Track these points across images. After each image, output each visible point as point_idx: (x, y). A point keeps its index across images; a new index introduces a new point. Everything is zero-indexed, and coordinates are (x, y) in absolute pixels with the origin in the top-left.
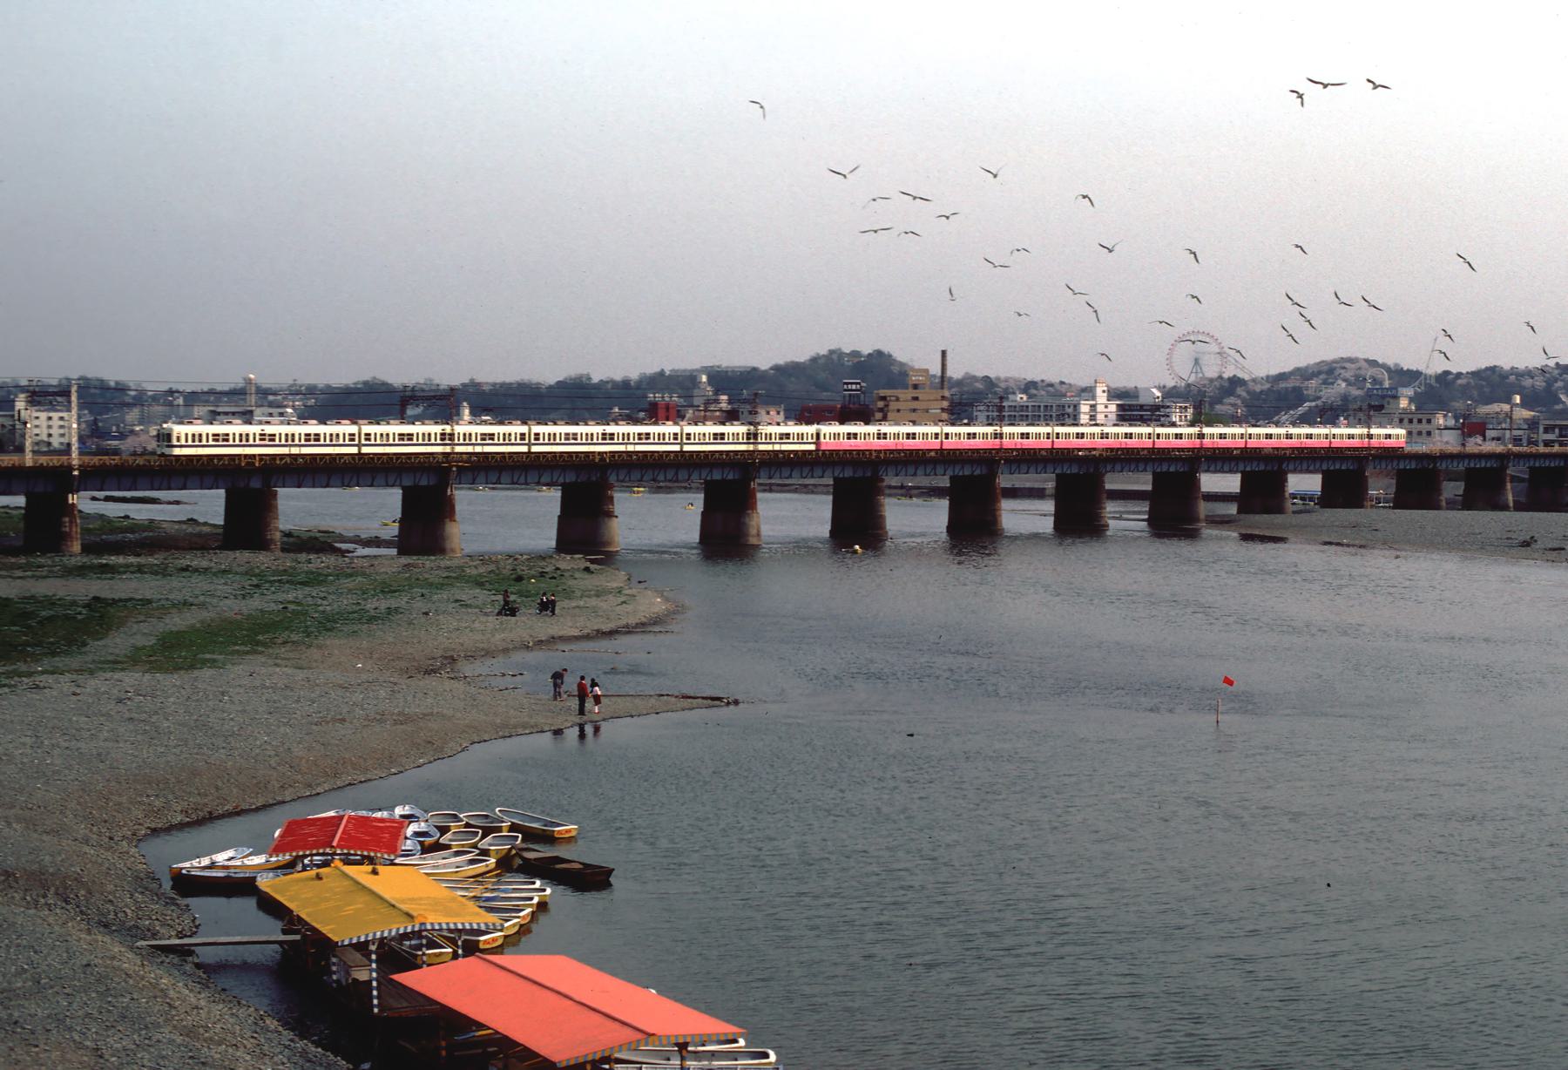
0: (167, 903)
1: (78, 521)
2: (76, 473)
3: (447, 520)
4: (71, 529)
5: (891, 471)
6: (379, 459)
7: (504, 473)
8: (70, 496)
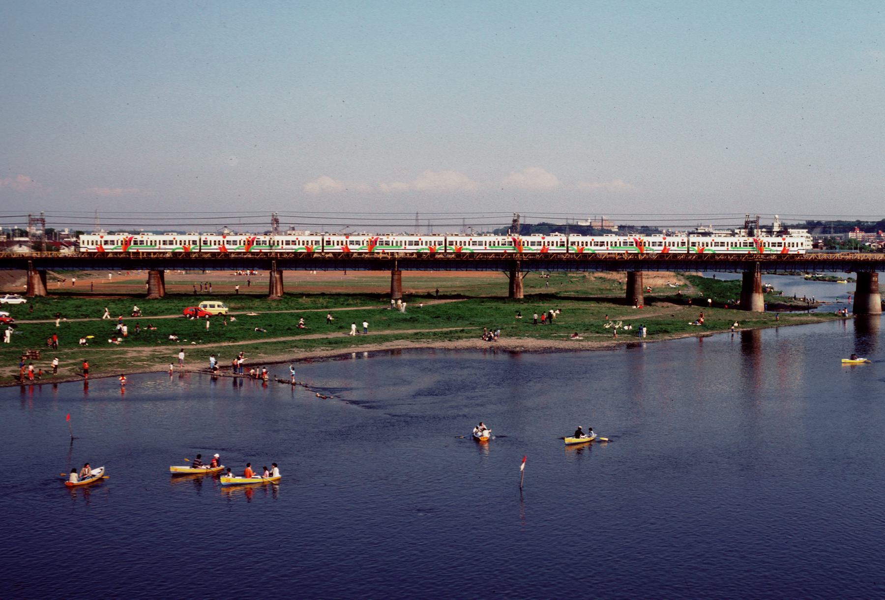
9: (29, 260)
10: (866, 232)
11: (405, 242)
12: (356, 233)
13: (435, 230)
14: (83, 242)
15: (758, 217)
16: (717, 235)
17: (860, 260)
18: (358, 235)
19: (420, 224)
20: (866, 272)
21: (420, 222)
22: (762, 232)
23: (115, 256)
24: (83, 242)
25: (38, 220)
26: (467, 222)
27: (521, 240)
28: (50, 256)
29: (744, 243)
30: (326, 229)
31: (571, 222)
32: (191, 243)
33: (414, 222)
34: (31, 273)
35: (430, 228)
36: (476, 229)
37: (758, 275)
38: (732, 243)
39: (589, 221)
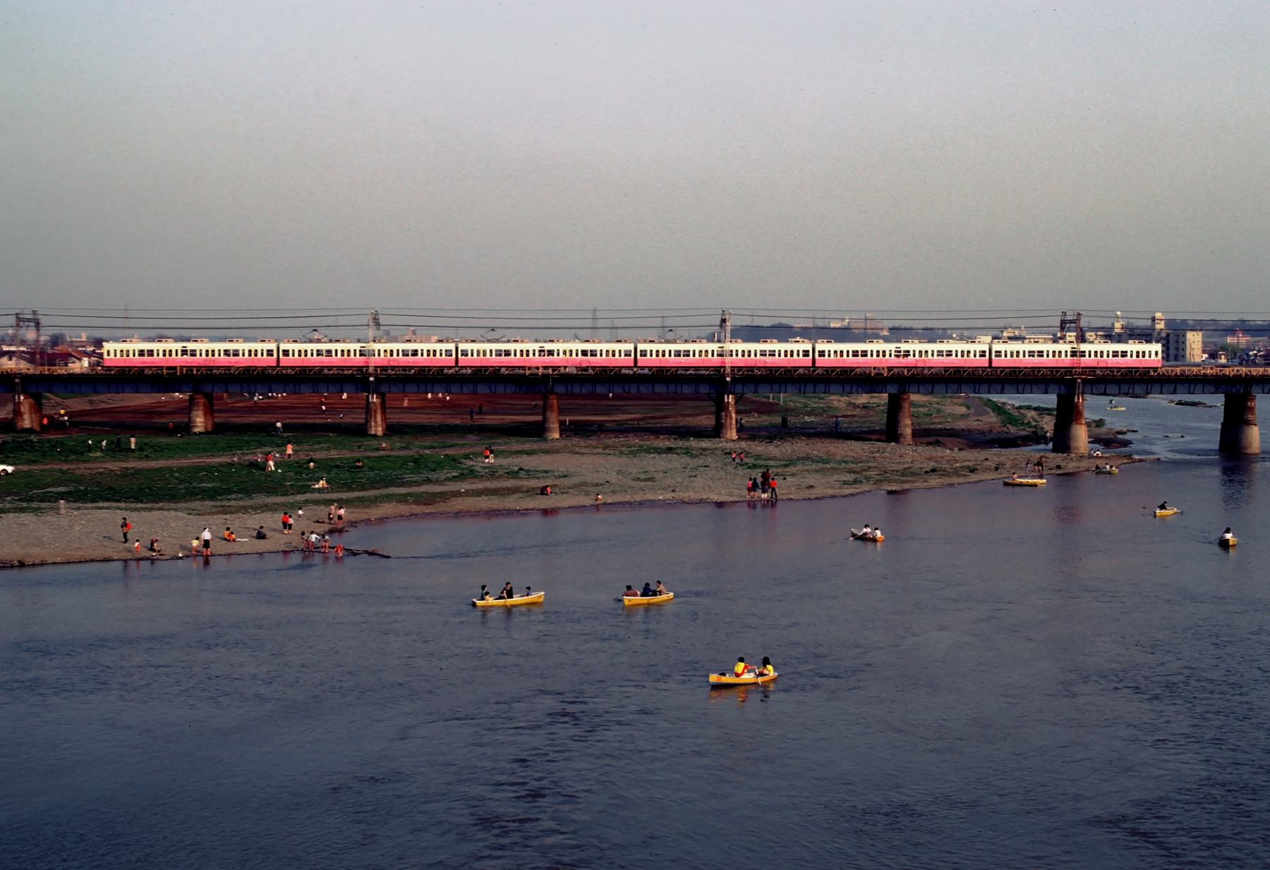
0: (480, 652)
1: (734, 416)
2: (372, 379)
3: (1074, 423)
4: (726, 421)
5: (914, 387)
6: (833, 371)
7: (936, 386)
8: (726, 396)
9: (17, 378)
10: (1253, 336)
11: (848, 352)
12: (506, 340)
13: (622, 334)
14: (108, 352)
15: (1079, 314)
16: (1032, 340)
17: (1229, 376)
18: (509, 341)
19: (599, 326)
20: (282, 394)
21: (600, 323)
22: (1097, 335)
23: (341, 372)
24: (108, 352)
25: (29, 320)
26: (668, 322)
27: (1071, 351)
28: (47, 373)
29: (896, 351)
30: (462, 332)
31: (820, 323)
32: (222, 353)
33: (588, 323)
34: (19, 398)
35: (614, 331)
36: (679, 332)
37: (1079, 399)
38: (878, 352)
39: (847, 321)
